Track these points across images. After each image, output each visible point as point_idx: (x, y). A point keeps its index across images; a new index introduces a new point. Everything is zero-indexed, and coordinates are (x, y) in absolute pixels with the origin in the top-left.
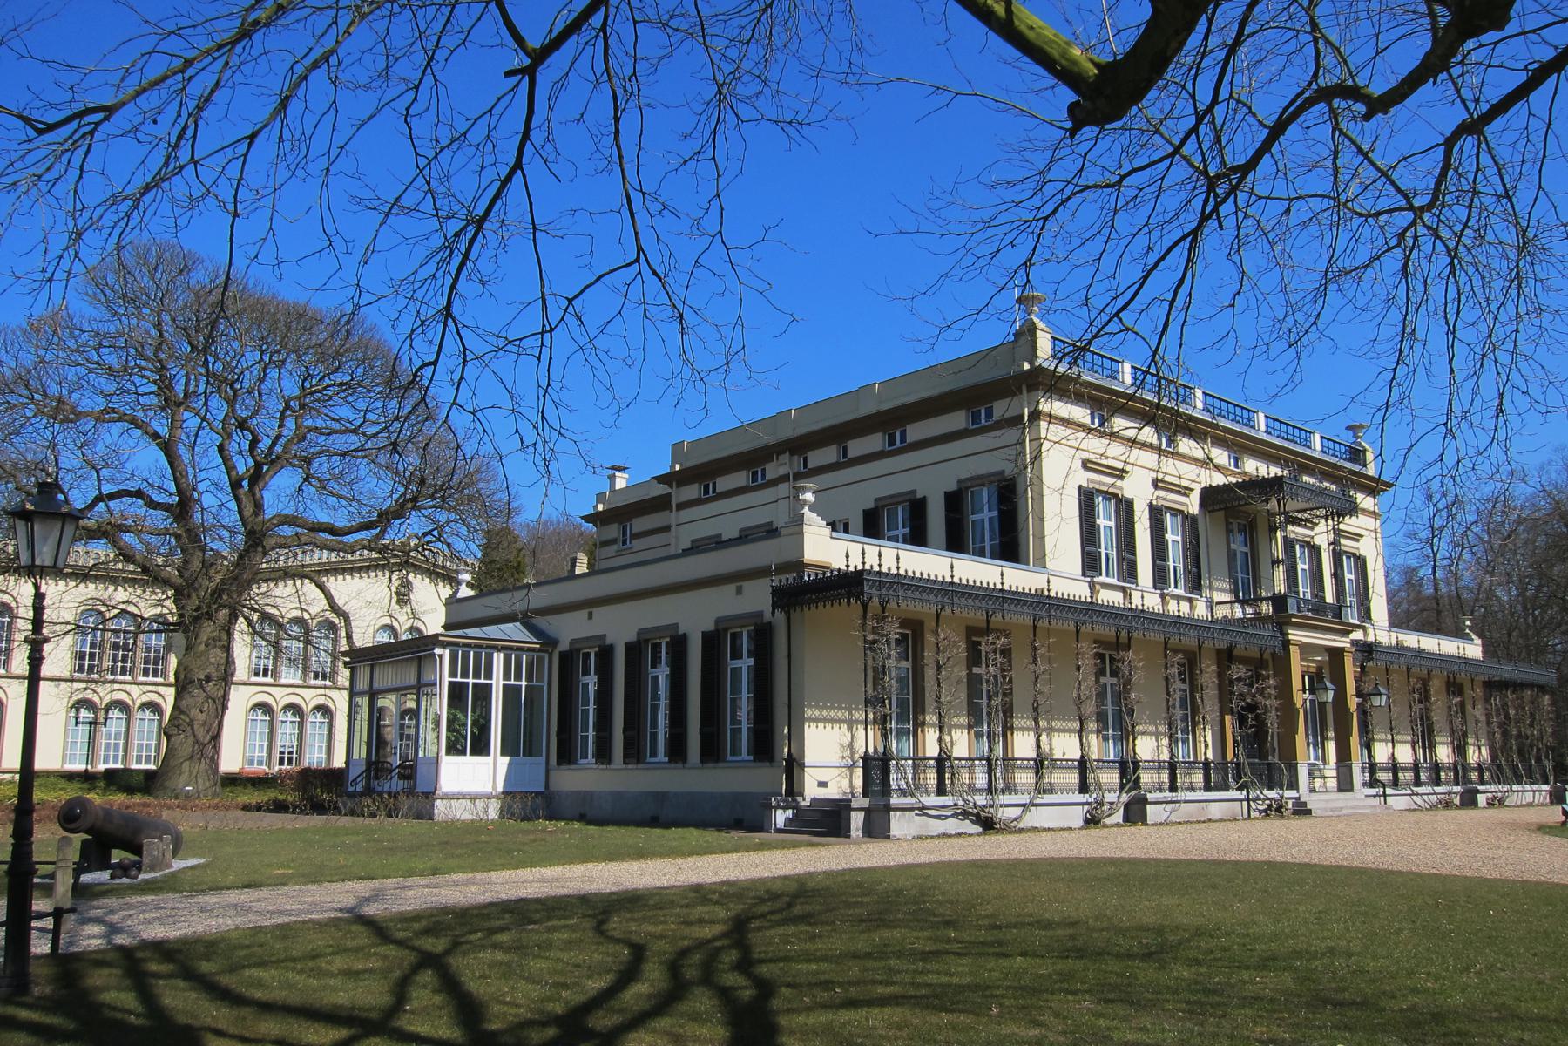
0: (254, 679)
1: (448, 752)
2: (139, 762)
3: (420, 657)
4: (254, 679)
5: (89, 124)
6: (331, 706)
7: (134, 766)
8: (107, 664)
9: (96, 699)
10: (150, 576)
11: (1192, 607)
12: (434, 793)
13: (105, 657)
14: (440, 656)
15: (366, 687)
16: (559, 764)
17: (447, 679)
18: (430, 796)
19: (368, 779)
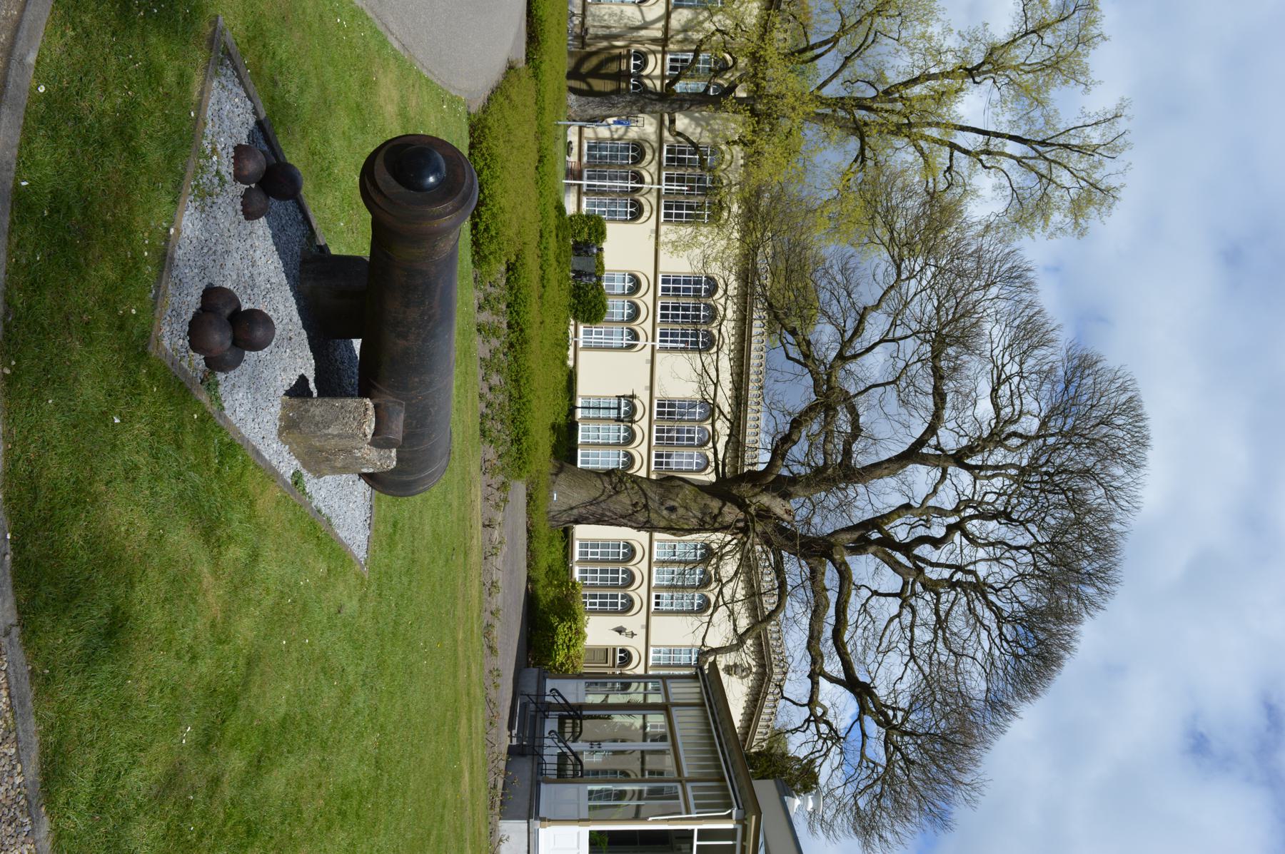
0: (655, 402)
1: (591, 832)
2: (583, 455)
3: (723, 779)
4: (655, 402)
5: (881, 117)
6: (643, 219)
7: (579, 452)
8: (666, 425)
9: (644, 163)
10: (780, 448)
11: (771, 701)
12: (537, 817)
13: (671, 424)
14: (729, 817)
15: (673, 699)
16: (591, 832)
17: (696, 827)
18: (532, 812)
19: (559, 707)
